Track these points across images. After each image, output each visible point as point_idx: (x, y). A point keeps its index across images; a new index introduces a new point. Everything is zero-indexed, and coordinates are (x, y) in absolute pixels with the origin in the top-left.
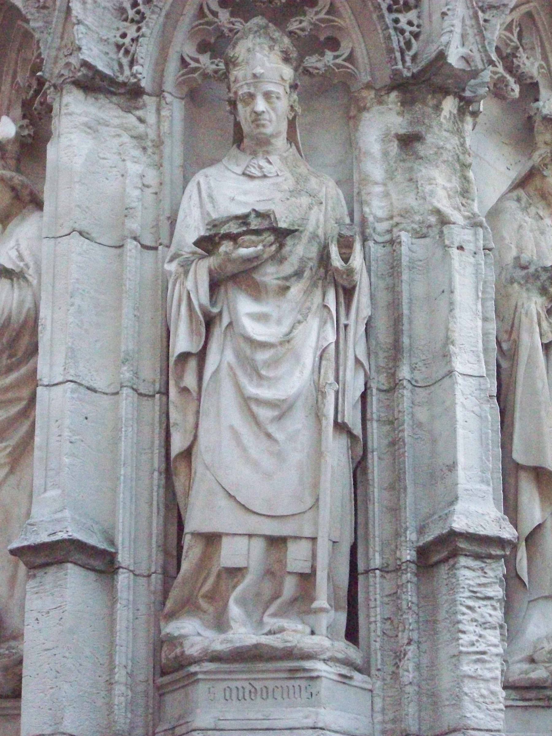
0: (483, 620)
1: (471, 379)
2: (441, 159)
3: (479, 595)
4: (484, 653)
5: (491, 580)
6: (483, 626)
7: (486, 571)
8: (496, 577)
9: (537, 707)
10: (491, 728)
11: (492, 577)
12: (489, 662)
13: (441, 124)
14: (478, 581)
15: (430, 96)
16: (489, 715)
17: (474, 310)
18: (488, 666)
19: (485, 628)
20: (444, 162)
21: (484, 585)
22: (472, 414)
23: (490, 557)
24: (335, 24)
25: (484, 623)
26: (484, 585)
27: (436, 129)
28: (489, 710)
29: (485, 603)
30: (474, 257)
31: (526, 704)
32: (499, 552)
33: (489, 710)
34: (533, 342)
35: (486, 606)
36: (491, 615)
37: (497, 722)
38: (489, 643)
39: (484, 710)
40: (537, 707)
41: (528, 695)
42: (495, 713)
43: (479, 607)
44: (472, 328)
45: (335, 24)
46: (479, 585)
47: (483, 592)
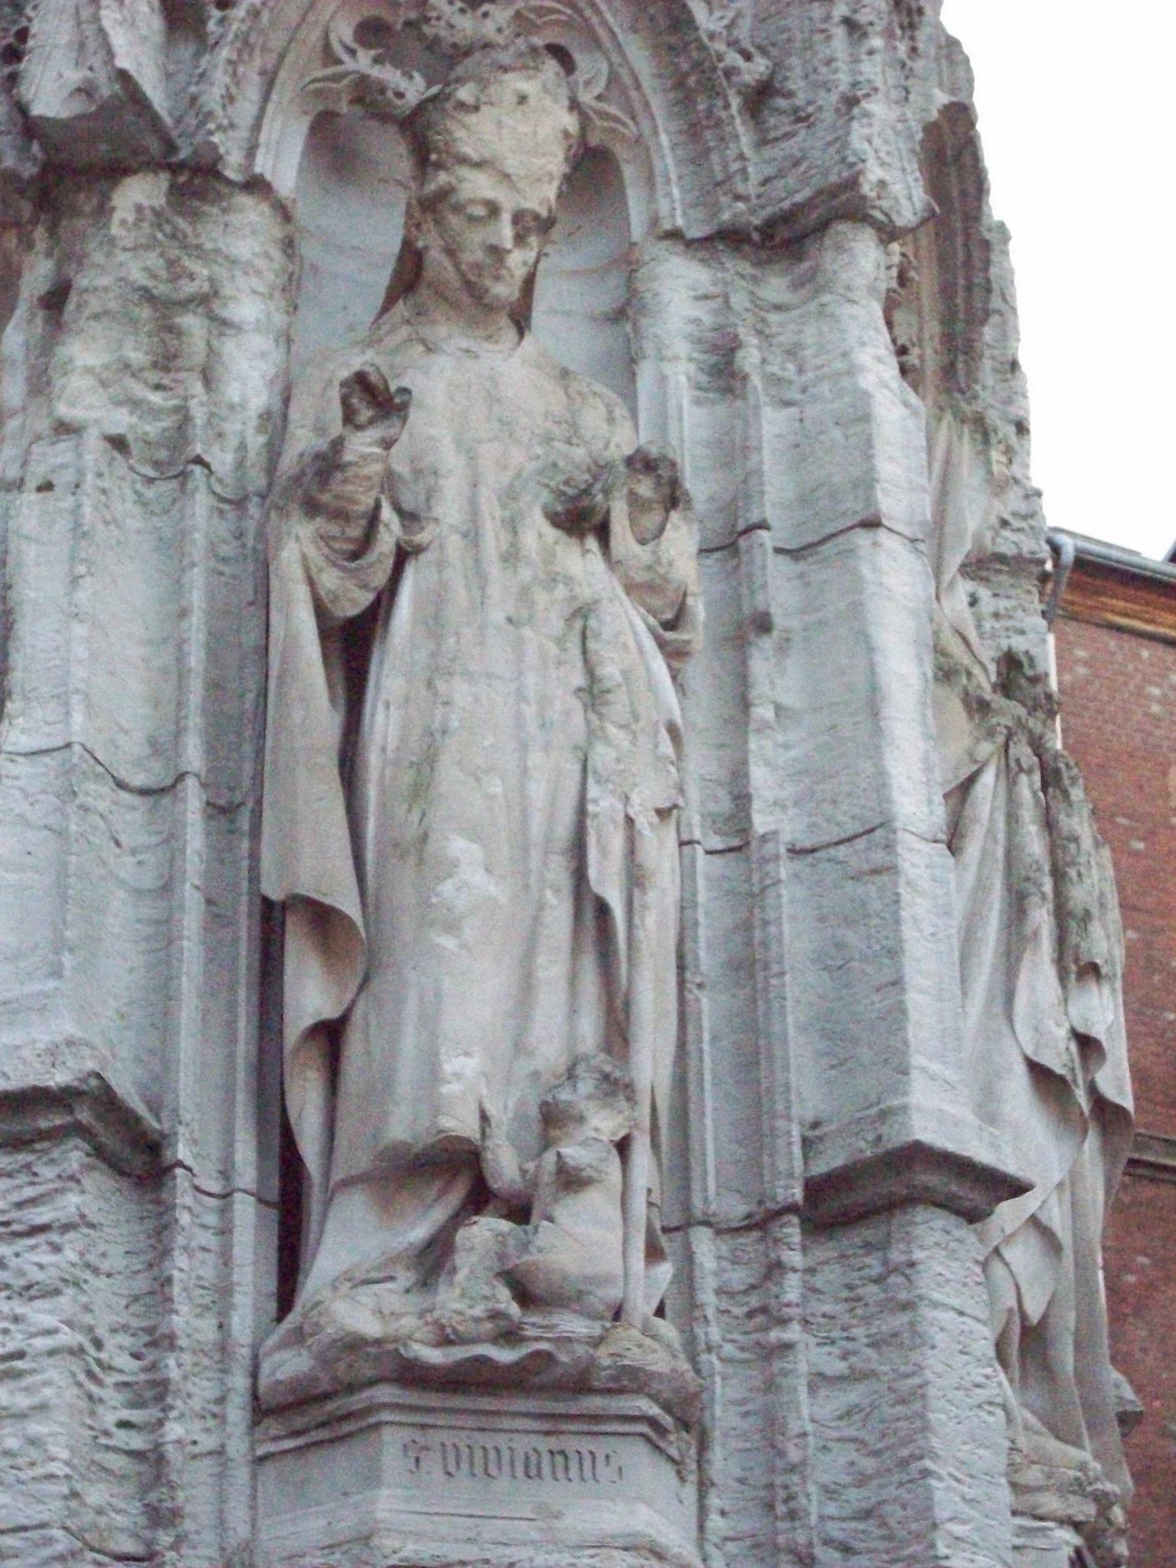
0: (22, 1282)
1: (47, 759)
2: (87, 313)
3: (16, 1227)
4: (20, 1355)
5: (52, 1186)
6: (26, 1294)
7: (35, 1169)
8: (60, 1176)
9: (318, 1444)
10: (26, 1522)
11: (52, 1181)
12: (32, 1372)
13: (112, 241)
14: (15, 1197)
15: (82, 196)
16: (23, 1494)
17: (65, 606)
18: (27, 1381)
19: (31, 1299)
20: (96, 317)
21: (33, 1201)
22: (46, 832)
23: (43, 1135)
24: (621, 128)
25: (29, 1287)
26: (33, 1201)
27: (98, 257)
28: (23, 1483)
29: (31, 1241)
30: (74, 494)
31: (300, 1441)
32: (58, 1120)
33: (23, 1483)
34: (1162, 624)
35: (33, 1248)
36: (41, 1266)
37: (40, 1507)
38: (33, 1330)
39: (10, 1486)
40: (318, 1444)
41: (299, 1422)
42: (39, 1486)
43: (17, 1255)
44: (57, 649)
45: (621, 128)
46: (20, 1205)
47: (24, 1219)
